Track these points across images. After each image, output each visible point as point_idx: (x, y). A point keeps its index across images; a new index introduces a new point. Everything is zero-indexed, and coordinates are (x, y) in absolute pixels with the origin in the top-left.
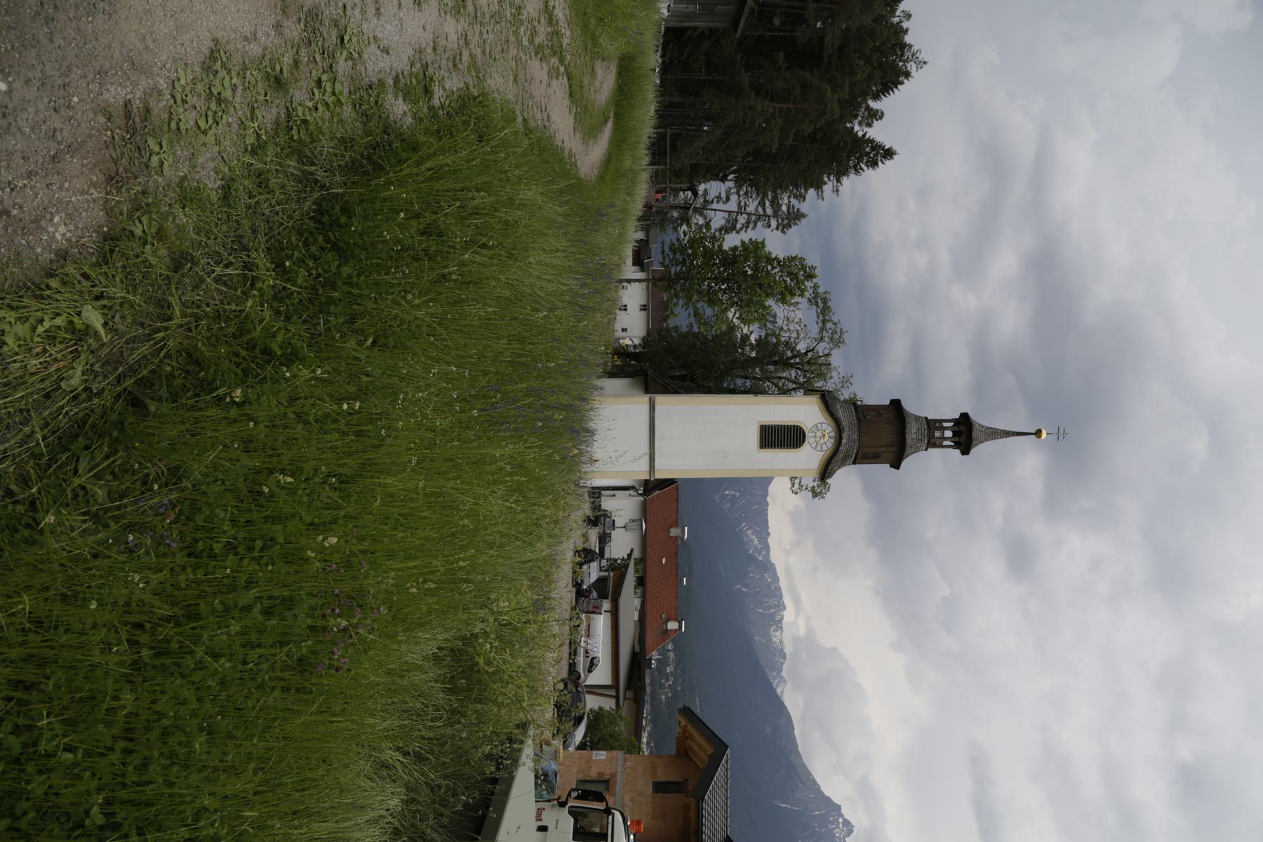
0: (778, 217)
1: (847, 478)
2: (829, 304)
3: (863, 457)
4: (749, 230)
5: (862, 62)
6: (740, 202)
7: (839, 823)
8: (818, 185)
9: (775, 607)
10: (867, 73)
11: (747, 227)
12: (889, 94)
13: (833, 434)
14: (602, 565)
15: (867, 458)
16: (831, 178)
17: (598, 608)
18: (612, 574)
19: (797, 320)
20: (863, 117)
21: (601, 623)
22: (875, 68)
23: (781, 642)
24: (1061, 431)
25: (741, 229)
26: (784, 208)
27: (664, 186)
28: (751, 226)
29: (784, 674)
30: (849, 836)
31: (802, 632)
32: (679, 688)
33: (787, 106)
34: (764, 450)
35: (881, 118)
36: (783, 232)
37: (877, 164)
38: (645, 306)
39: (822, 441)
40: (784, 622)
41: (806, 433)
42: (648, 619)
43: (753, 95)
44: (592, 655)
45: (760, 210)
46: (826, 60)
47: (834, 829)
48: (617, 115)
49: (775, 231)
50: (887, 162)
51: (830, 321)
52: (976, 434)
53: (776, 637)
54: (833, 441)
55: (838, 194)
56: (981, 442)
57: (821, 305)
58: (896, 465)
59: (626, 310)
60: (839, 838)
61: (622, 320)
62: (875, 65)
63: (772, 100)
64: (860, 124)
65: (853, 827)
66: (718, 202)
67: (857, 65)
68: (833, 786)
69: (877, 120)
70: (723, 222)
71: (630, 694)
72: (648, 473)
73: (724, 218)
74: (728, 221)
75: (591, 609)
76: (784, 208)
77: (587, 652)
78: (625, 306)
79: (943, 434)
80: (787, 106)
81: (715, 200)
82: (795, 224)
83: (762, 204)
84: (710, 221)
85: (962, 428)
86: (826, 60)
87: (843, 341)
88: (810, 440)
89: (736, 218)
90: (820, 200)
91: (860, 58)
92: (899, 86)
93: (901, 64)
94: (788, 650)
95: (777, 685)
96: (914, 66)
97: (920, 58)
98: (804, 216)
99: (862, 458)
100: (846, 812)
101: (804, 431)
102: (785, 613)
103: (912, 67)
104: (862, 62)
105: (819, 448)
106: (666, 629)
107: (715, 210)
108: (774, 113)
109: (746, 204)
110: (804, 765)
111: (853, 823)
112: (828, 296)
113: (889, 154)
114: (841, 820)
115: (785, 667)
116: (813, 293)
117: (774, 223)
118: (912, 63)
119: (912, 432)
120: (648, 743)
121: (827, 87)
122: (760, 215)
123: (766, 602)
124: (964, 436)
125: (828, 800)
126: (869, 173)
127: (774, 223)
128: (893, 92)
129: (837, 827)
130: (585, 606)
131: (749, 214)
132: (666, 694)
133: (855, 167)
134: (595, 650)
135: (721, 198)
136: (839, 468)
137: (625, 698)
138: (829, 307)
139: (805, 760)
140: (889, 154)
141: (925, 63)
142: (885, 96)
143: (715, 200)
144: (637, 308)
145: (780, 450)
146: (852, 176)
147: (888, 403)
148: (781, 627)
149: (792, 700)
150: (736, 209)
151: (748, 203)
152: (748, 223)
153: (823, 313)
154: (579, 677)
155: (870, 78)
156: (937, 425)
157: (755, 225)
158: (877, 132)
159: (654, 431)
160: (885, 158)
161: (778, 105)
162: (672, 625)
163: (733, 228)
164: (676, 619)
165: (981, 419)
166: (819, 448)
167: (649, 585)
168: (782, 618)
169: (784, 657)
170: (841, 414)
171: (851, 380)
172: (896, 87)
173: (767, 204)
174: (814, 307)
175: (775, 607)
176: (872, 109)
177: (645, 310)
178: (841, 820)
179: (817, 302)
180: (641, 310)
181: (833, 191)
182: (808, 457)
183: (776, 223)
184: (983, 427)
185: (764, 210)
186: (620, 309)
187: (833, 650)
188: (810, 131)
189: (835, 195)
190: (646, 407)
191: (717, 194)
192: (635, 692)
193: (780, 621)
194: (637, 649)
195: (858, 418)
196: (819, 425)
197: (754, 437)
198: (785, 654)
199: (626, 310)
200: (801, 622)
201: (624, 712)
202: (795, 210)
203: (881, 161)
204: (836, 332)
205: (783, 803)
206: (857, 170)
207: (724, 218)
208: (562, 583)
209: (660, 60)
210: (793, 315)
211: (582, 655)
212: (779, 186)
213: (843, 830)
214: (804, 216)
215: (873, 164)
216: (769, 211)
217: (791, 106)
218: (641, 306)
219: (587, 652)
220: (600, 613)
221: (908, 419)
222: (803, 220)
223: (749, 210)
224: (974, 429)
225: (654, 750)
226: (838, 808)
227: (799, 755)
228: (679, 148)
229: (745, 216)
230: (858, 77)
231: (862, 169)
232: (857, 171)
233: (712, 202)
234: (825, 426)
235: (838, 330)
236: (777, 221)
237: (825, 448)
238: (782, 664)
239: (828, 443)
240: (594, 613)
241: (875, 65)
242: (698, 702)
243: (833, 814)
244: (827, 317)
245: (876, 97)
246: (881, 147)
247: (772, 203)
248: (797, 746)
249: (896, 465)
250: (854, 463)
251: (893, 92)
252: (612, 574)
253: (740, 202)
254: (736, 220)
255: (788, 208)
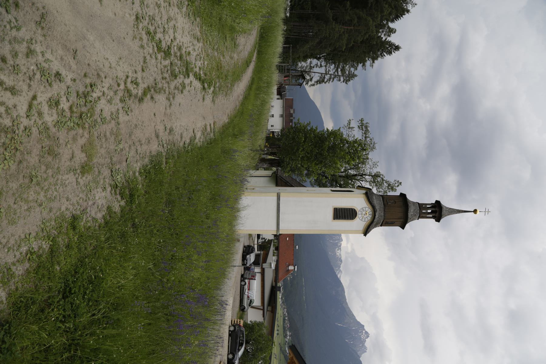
0: (344, 76)
1: (377, 232)
2: (369, 129)
3: (385, 223)
4: (330, 82)
5: (387, 6)
6: (326, 69)
7: (363, 333)
8: (364, 62)
9: (338, 240)
10: (389, 11)
11: (329, 81)
12: (398, 20)
13: (371, 213)
14: (259, 242)
15: (387, 224)
16: (370, 59)
17: (254, 276)
18: (262, 252)
19: (352, 136)
20: (386, 32)
21: (256, 284)
22: (393, 9)
23: (340, 255)
24: (487, 210)
25: (327, 81)
26: (347, 73)
27: (289, 74)
28: (331, 80)
29: (341, 269)
30: (367, 338)
31: (350, 250)
32: (296, 274)
33: (350, 28)
34: (335, 220)
35: (395, 32)
36: (346, 83)
37: (391, 53)
38: (282, 115)
39: (365, 217)
40: (342, 246)
41: (357, 212)
42: (280, 266)
43: (334, 23)
44: (250, 298)
45: (336, 73)
46: (370, 5)
47: (361, 335)
48: (260, 53)
49: (342, 83)
50: (396, 52)
51: (369, 137)
52: (444, 212)
53: (338, 253)
54: (371, 216)
55: (372, 67)
56: (446, 216)
57: (364, 129)
58: (403, 227)
59: (273, 117)
60: (363, 339)
61: (272, 121)
62: (393, 7)
63: (343, 24)
64: (385, 35)
65: (369, 334)
66: (316, 67)
67: (385, 7)
68: (361, 316)
69: (393, 33)
70: (318, 78)
71: (270, 308)
72: (276, 232)
73: (319, 76)
74: (321, 78)
75: (250, 277)
76: (347, 73)
77: (248, 297)
78: (273, 115)
79: (427, 211)
80: (350, 28)
81: (315, 66)
82: (352, 80)
83: (337, 70)
84: (312, 78)
85: (437, 209)
86: (370, 5)
87: (375, 148)
88: (359, 216)
89: (324, 77)
90: (364, 70)
91: (386, 4)
92: (403, 16)
93: (404, 5)
94: (343, 258)
95: (338, 274)
96: (410, 6)
97: (414, 2)
98: (356, 76)
99: (385, 224)
100: (367, 328)
101: (356, 211)
102: (342, 242)
103: (410, 7)
104: (387, 6)
105: (363, 220)
106: (288, 269)
107: (315, 72)
108: (344, 31)
109: (329, 70)
110: (349, 308)
111: (369, 333)
112: (368, 125)
113: (397, 48)
114: (364, 331)
115: (341, 265)
116: (361, 123)
117: (342, 79)
118: (410, 4)
119: (412, 211)
120: (282, 298)
121: (369, 18)
122: (335, 75)
123: (334, 238)
124: (438, 213)
125: (359, 323)
126: (387, 57)
127: (342, 79)
128: (400, 19)
129: (362, 334)
130: (247, 275)
131: (331, 75)
132: (290, 277)
133: (381, 54)
134: (252, 296)
135: (318, 65)
136: (373, 228)
137: (267, 311)
138: (368, 130)
139: (350, 305)
140: (397, 48)
141: (416, 4)
142: (397, 20)
143: (315, 66)
144: (278, 116)
145: (344, 221)
146: (379, 59)
147: (399, 195)
148: (340, 249)
149: (344, 279)
150: (324, 72)
151: (330, 70)
152: (330, 79)
153: (365, 133)
154: (245, 308)
155: (390, 14)
156: (424, 206)
157: (333, 80)
158: (393, 39)
159: (279, 208)
160: (395, 50)
161: (346, 28)
162: (291, 268)
163: (323, 81)
164: (293, 265)
165: (446, 203)
166: (363, 220)
167: (280, 250)
168: (341, 245)
169: (341, 261)
170: (376, 202)
171: (378, 164)
172: (402, 16)
173: (339, 70)
174: (361, 131)
175: (338, 240)
176: (390, 28)
177: (282, 117)
178: (364, 331)
179: (362, 128)
180: (280, 117)
181: (370, 66)
182: (359, 223)
183: (343, 79)
184: (447, 208)
185: (338, 73)
186: (270, 117)
187: (363, 259)
188: (361, 40)
189: (371, 67)
190: (275, 198)
191: (316, 63)
192: (272, 308)
193: (340, 246)
194: (274, 285)
195: (384, 204)
196: (364, 208)
197: (330, 213)
198: (342, 260)
199: (273, 117)
200: (349, 246)
201: (266, 324)
202: (352, 73)
203: (394, 51)
204: (372, 144)
205: (339, 324)
206: (382, 56)
207: (319, 76)
208: (233, 279)
209: (289, 4)
210: (351, 133)
211: (246, 298)
212: (345, 62)
213: (365, 336)
214: (356, 76)
215: (390, 53)
216: (340, 73)
217: (352, 28)
218: (280, 115)
219: (248, 297)
220: (255, 279)
221: (409, 205)
222: (355, 78)
223: (330, 73)
224: (443, 210)
225: (284, 301)
226: (363, 326)
227: (347, 304)
228: (298, 48)
229: (329, 76)
230: (385, 13)
231: (384, 55)
232: (382, 56)
233: (314, 67)
234: (367, 209)
235: (373, 142)
236: (344, 78)
237: (366, 220)
238: (341, 264)
239: (369, 217)
240: (252, 279)
241: (393, 7)
242: (303, 280)
243: (361, 329)
244: (367, 136)
245: (392, 21)
246: (394, 45)
247: (341, 70)
248: (346, 300)
249: (403, 227)
250: (381, 226)
251: (400, 19)
252: (262, 252)
253: (326, 69)
254: (324, 78)
255: (349, 73)
